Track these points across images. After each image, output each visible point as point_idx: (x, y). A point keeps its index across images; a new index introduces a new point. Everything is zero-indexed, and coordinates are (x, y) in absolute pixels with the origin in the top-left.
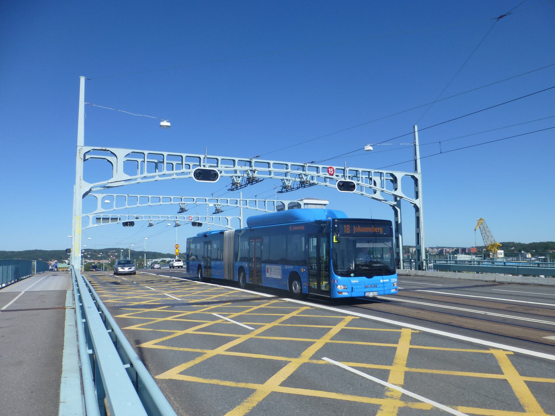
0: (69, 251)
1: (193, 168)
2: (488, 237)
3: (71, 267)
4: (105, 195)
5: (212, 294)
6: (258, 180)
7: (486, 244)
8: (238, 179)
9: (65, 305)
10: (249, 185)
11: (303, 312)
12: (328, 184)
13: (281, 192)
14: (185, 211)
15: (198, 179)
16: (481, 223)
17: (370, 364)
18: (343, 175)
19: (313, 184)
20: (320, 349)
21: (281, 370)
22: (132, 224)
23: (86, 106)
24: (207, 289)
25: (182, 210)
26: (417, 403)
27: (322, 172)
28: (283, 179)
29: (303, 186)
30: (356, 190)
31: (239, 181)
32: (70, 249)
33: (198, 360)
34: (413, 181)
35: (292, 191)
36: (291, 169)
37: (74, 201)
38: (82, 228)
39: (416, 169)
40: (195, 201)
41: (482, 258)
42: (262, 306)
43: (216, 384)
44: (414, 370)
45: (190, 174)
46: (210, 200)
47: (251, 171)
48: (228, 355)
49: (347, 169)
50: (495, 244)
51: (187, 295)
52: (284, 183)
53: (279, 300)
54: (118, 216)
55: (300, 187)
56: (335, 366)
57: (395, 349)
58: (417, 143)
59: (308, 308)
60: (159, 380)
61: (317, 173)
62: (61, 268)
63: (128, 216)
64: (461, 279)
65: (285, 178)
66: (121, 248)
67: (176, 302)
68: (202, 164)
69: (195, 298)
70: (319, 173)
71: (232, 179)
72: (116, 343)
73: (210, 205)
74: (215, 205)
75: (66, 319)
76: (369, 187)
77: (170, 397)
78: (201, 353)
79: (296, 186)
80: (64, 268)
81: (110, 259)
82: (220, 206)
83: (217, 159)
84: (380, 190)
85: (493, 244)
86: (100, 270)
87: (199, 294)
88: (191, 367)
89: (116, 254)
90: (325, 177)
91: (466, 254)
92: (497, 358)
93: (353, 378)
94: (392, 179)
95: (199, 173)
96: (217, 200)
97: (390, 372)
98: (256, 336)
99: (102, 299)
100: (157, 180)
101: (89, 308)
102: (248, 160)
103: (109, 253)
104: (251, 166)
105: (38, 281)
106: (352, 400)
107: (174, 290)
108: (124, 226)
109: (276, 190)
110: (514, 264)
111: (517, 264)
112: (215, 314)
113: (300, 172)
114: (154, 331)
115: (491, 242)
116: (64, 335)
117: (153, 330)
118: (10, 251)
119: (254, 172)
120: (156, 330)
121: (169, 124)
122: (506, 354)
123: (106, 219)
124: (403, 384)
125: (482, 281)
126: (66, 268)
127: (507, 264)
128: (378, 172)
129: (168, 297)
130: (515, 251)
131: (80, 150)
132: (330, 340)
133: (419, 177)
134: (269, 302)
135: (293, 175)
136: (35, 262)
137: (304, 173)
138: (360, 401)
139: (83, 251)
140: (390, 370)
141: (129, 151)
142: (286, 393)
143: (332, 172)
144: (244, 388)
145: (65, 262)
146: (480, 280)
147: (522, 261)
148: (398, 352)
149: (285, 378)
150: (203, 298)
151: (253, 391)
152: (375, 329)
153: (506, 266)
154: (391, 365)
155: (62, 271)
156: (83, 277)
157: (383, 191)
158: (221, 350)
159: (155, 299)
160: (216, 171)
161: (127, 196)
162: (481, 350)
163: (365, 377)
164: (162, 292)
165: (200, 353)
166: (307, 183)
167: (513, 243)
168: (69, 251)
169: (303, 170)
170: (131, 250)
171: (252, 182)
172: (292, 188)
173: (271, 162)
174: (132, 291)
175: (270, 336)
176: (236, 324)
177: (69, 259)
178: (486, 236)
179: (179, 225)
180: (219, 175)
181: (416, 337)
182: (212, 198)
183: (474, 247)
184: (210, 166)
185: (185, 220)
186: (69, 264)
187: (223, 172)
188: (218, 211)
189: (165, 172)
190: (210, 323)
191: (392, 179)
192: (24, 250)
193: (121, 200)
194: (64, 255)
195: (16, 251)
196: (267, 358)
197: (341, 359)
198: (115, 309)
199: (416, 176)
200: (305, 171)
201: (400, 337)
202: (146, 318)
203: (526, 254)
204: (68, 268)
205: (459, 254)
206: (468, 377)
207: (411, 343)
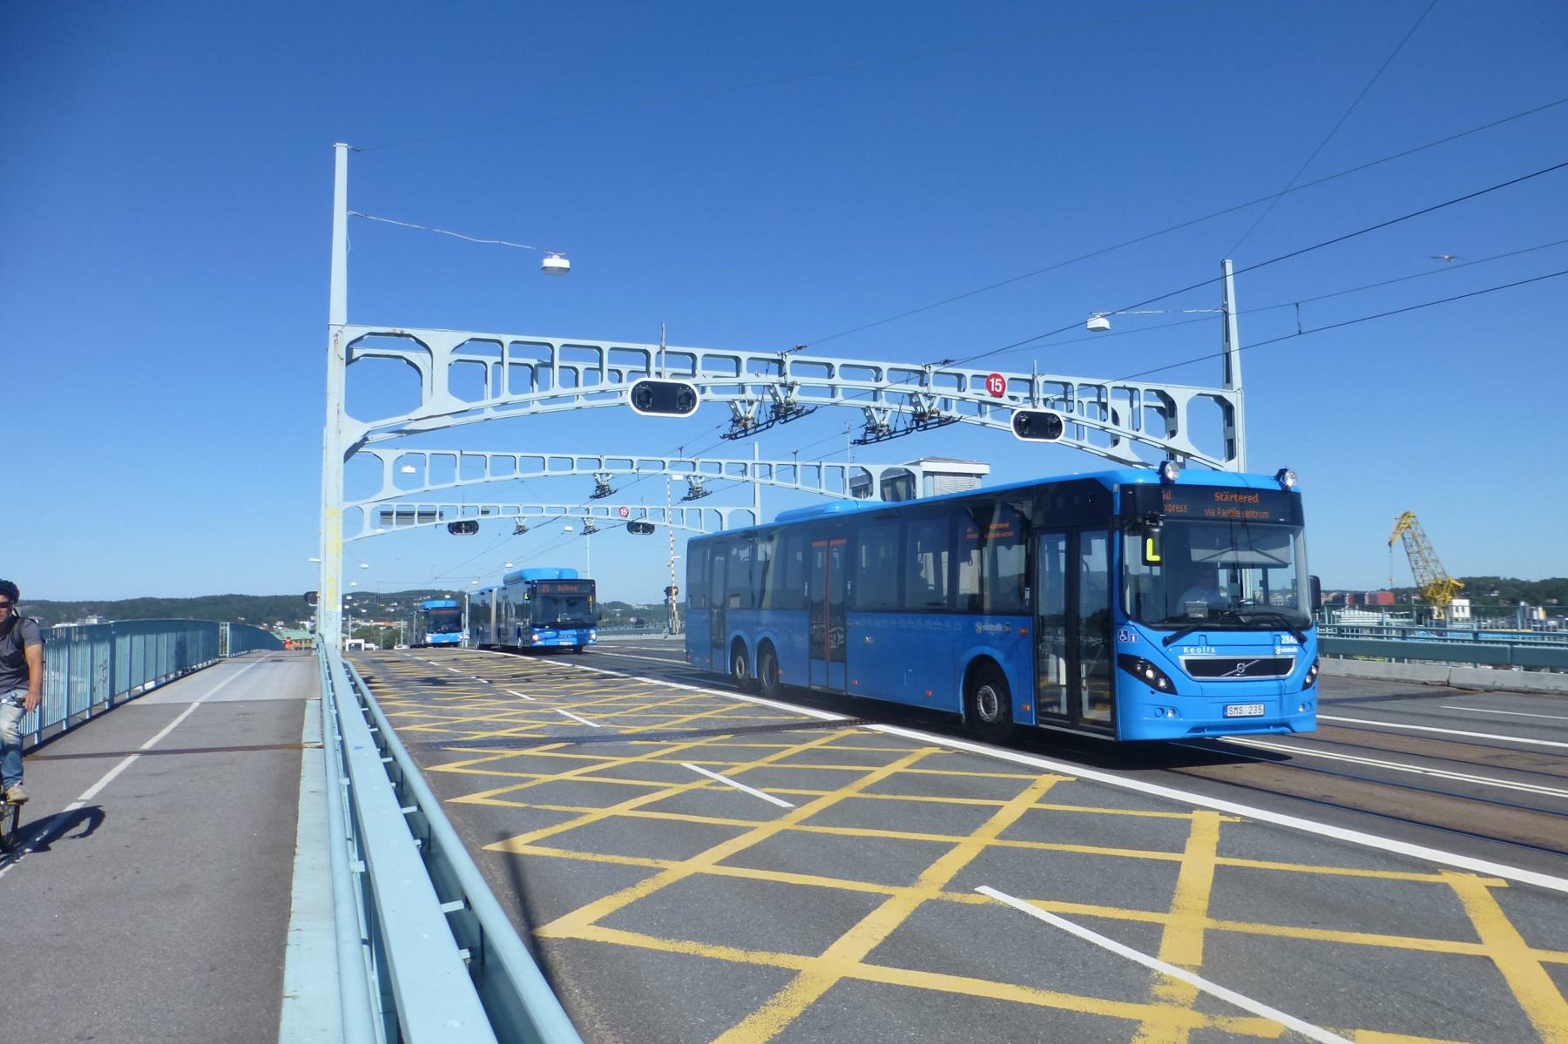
0: (311, 597)
1: (630, 380)
2: (1427, 562)
4: (402, 452)
6: (802, 410)
7: (1421, 581)
8: (748, 408)
9: (300, 740)
10: (777, 422)
11: (923, 763)
12: (987, 419)
13: (863, 442)
14: (611, 493)
15: (643, 409)
16: (1406, 526)
18: (1028, 395)
19: (949, 421)
20: (971, 862)
21: (866, 919)
22: (472, 527)
23: (351, 222)
25: (602, 492)
26: (1241, 1018)
27: (972, 387)
28: (868, 407)
31: (752, 412)
33: (644, 889)
34: (1219, 411)
35: (891, 438)
36: (890, 379)
37: (324, 469)
39: (1228, 379)
41: (1412, 620)
42: (814, 745)
44: (1230, 926)
46: (674, 465)
47: (782, 385)
48: (723, 876)
49: (1041, 380)
50: (1445, 582)
51: (617, 714)
52: (871, 417)
53: (859, 729)
54: (438, 506)
55: (912, 429)
56: (1011, 909)
57: (1176, 866)
58: (1232, 309)
59: (936, 750)
61: (959, 390)
63: (463, 507)
65: (872, 404)
66: (445, 589)
67: (586, 733)
68: (653, 369)
69: (637, 722)
70: (964, 390)
71: (733, 407)
72: (430, 852)
73: (675, 477)
74: (688, 477)
75: (302, 774)
77: (570, 988)
78: (653, 869)
79: (901, 427)
83: (693, 356)
84: (1131, 437)
85: (1440, 582)
87: (646, 711)
88: (625, 907)
90: (980, 401)
91: (1363, 608)
92: (1461, 897)
93: (1063, 945)
94: (1162, 404)
95: (647, 392)
96: (694, 463)
97: (1165, 930)
98: (797, 824)
101: (357, 748)
102: (775, 357)
104: (781, 373)
105: (226, 682)
106: (1060, 1007)
108: (452, 532)
109: (850, 438)
110: (1500, 637)
111: (1509, 636)
113: (913, 387)
114: (531, 808)
115: (1435, 578)
116: (296, 818)
117: (527, 805)
119: (791, 389)
120: (534, 807)
121: (565, 264)
122: (1487, 887)
123: (405, 515)
124: (1200, 964)
125: (1412, 682)
126: (306, 640)
127: (1483, 637)
128: (1125, 388)
129: (565, 718)
130: (1501, 601)
131: (337, 335)
132: (996, 838)
134: (830, 735)
135: (893, 396)
136: (226, 625)
137: (925, 390)
138: (1084, 1010)
139: (349, 598)
140: (1162, 925)
141: (464, 336)
143: (998, 387)
144: (768, 966)
145: (304, 626)
146: (1406, 681)
148: (1184, 873)
149: (876, 940)
151: (792, 974)
152: (1120, 812)
153: (1481, 642)
154: (1166, 910)
156: (345, 666)
157: (1137, 438)
158: (705, 863)
160: (690, 388)
161: (458, 454)
162: (1415, 872)
163: (1094, 944)
166: (931, 418)
167: (1497, 579)
168: (311, 597)
169: (921, 384)
171: (785, 417)
172: (893, 430)
173: (837, 363)
175: (835, 826)
176: (744, 793)
177: (312, 618)
179: (595, 531)
180: (699, 397)
181: (1233, 836)
182: (679, 459)
184: (674, 375)
185: (609, 517)
187: (708, 390)
188: (695, 494)
189: (556, 390)
190: (676, 789)
191: (1162, 404)
194: (301, 607)
197: (1029, 891)
198: (429, 751)
199: (1229, 396)
200: (926, 385)
201: (1188, 835)
202: (509, 774)
203: (1532, 610)
204: (311, 641)
205: (1342, 609)
206: (1381, 948)
207: (1220, 851)
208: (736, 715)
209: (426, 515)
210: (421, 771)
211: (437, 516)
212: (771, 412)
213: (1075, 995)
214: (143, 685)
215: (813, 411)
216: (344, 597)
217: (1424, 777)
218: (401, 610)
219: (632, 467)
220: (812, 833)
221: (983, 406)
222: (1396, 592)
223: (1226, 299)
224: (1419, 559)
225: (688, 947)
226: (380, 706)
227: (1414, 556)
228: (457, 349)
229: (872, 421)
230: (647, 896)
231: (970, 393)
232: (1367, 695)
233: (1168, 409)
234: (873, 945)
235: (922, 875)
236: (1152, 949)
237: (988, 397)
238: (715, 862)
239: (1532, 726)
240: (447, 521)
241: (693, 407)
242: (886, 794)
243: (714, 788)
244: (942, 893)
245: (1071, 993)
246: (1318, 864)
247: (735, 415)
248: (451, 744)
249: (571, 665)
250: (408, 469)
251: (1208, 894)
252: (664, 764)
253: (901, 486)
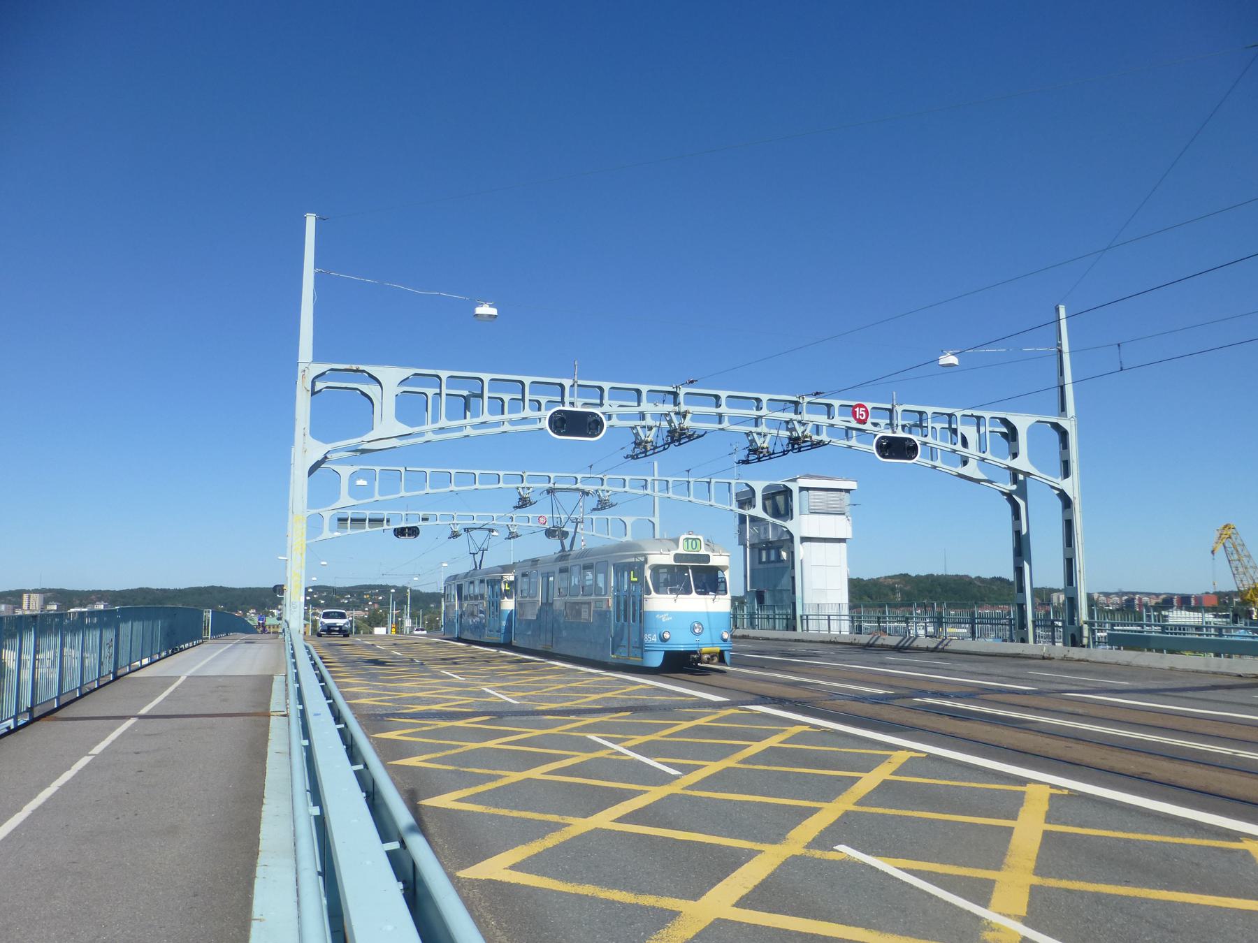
0: (279, 589)
1: (548, 409)
2: (1246, 568)
3: (284, 625)
5: (588, 691)
6: (694, 434)
8: (648, 433)
9: (269, 709)
10: (672, 445)
11: (795, 739)
12: (853, 442)
13: (746, 462)
14: (531, 504)
15: (559, 433)
16: (1227, 536)
17: (949, 864)
18: (888, 422)
19: (820, 444)
20: (832, 825)
22: (414, 532)
23: (317, 276)
24: (578, 681)
25: (524, 503)
28: (751, 432)
29: (796, 449)
30: (921, 457)
31: (651, 435)
32: (283, 585)
33: (552, 840)
34: (1055, 436)
35: (771, 458)
37: (292, 481)
38: (307, 540)
39: (1063, 408)
40: (552, 481)
41: (1228, 620)
42: (701, 722)
43: (590, 894)
45: (540, 422)
47: (677, 413)
49: (899, 409)
51: (533, 693)
52: (753, 441)
54: (385, 514)
55: (788, 451)
56: (865, 865)
57: (1010, 831)
59: (806, 728)
60: (466, 882)
61: (829, 418)
63: (407, 515)
64: (1177, 670)
65: (754, 429)
67: (506, 709)
68: (567, 399)
69: (549, 700)
70: (833, 418)
71: (634, 432)
75: (269, 738)
76: (949, 450)
79: (779, 449)
81: (367, 609)
82: (607, 494)
84: (978, 458)
87: (559, 690)
88: (535, 855)
89: (381, 598)
91: (1189, 609)
93: (907, 896)
94: (1005, 430)
96: (602, 479)
97: (996, 886)
98: (683, 789)
99: (346, 697)
100: (468, 436)
101: (316, 715)
102: (671, 389)
103: (366, 595)
104: (676, 403)
107: (502, 682)
108: (397, 536)
109: (736, 458)
112: (593, 737)
113: (790, 415)
117: (456, 768)
118: (159, 588)
119: (684, 417)
120: (462, 769)
123: (358, 521)
124: (1025, 914)
125: (1228, 675)
126: (274, 626)
128: (972, 416)
129: (489, 695)
133: (1071, 426)
134: (715, 713)
136: (209, 612)
137: (799, 417)
139: (310, 590)
140: (994, 881)
141: (409, 372)
142: (748, 924)
143: (862, 415)
144: (654, 907)
145: (273, 614)
146: (1222, 674)
149: (747, 888)
150: (567, 699)
151: (674, 915)
154: (998, 868)
156: (307, 648)
157: (983, 460)
158: (604, 820)
159: (463, 700)
160: (598, 416)
161: (403, 470)
163: (934, 896)
164: (478, 685)
165: (557, 823)
168: (279, 589)
169: (796, 412)
170: (413, 588)
171: (679, 440)
172: (772, 452)
173: (723, 394)
174: (413, 681)
175: (716, 791)
176: (639, 761)
177: (280, 607)
178: (1239, 566)
179: (517, 536)
180: (606, 423)
181: (1061, 805)
183: (1211, 592)
184: (585, 404)
186: (279, 619)
187: (614, 417)
189: (486, 417)
190: (582, 757)
191: (1005, 430)
193: (390, 480)
194: (271, 598)
196: (707, 842)
197: (880, 850)
198: (375, 720)
199: (1064, 423)
206: (1184, 904)
207: (1049, 818)
208: (634, 695)
209: (376, 521)
210: (368, 737)
211: (385, 522)
212: (667, 436)
213: (915, 937)
214: (130, 665)
215: (703, 436)
216: (306, 589)
217: (1233, 758)
218: (353, 601)
219: (549, 482)
220: (695, 797)
221: (850, 431)
222: (1220, 595)
223: (1060, 339)
224: (1239, 566)
225: (587, 890)
226: (335, 682)
227: (1235, 564)
228: (402, 382)
229: (754, 444)
230: (554, 846)
231: (838, 420)
232: (1188, 685)
233: (1011, 434)
234: (744, 892)
235: (789, 834)
236: (984, 901)
237: (854, 424)
238: (613, 819)
240: (393, 527)
241: (601, 432)
243: (614, 757)
244: (805, 850)
245: (911, 936)
246: (1133, 831)
247: (637, 438)
248: (394, 715)
249: (495, 650)
250: (361, 482)
251: (1036, 855)
252: (572, 736)
253: (780, 499)
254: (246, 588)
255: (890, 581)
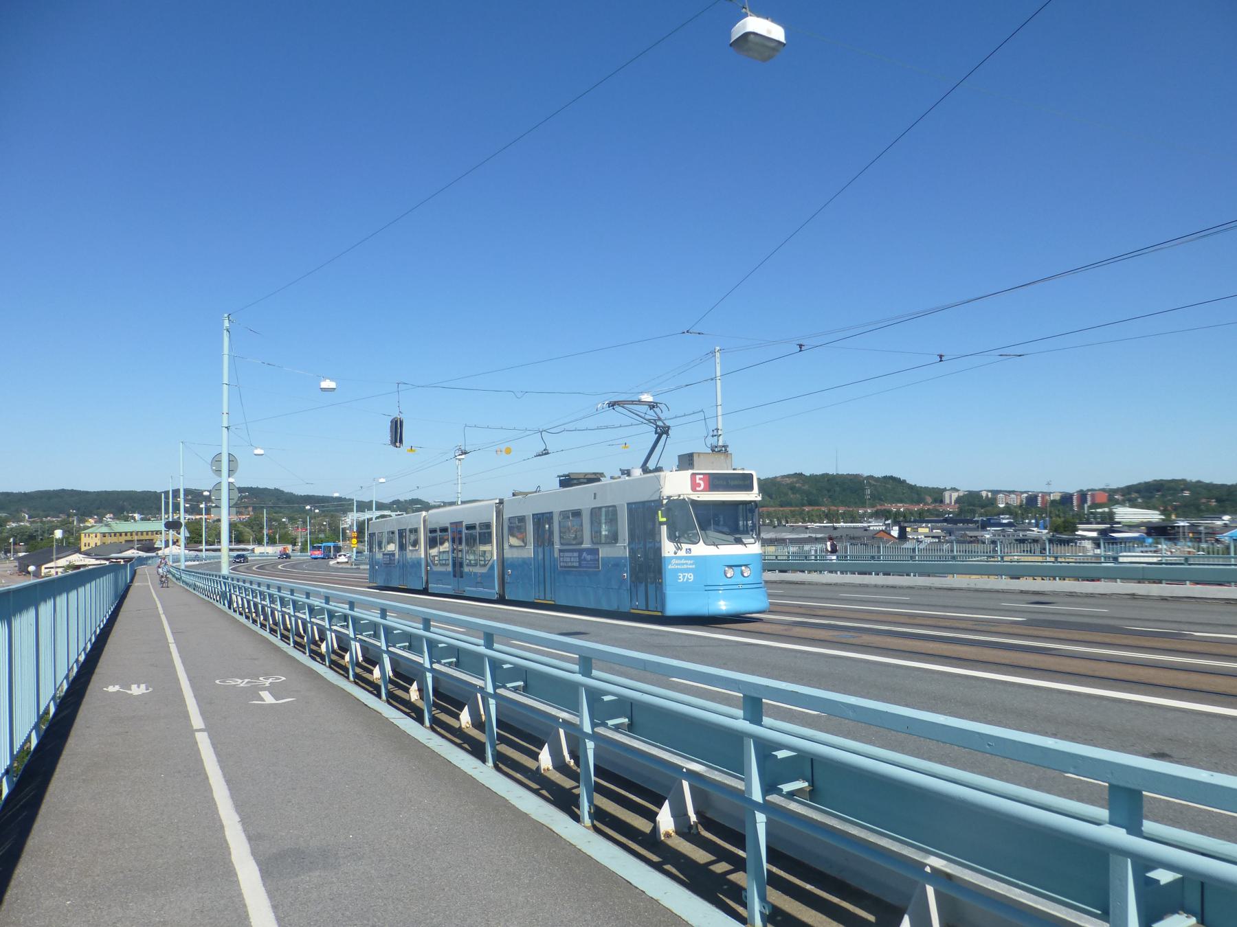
62: (123, 534)
80: (131, 535)
86: (231, 542)
145: (134, 518)
147: (1017, 552)
155: (126, 541)
167: (1184, 480)
192: (33, 490)
195: (15, 492)
239: (882, 602)
242: (676, 868)
254: (102, 492)
255: (788, 481)
